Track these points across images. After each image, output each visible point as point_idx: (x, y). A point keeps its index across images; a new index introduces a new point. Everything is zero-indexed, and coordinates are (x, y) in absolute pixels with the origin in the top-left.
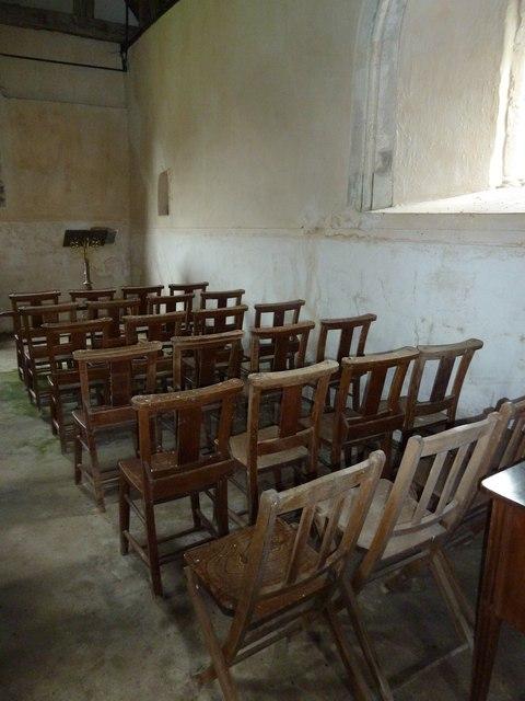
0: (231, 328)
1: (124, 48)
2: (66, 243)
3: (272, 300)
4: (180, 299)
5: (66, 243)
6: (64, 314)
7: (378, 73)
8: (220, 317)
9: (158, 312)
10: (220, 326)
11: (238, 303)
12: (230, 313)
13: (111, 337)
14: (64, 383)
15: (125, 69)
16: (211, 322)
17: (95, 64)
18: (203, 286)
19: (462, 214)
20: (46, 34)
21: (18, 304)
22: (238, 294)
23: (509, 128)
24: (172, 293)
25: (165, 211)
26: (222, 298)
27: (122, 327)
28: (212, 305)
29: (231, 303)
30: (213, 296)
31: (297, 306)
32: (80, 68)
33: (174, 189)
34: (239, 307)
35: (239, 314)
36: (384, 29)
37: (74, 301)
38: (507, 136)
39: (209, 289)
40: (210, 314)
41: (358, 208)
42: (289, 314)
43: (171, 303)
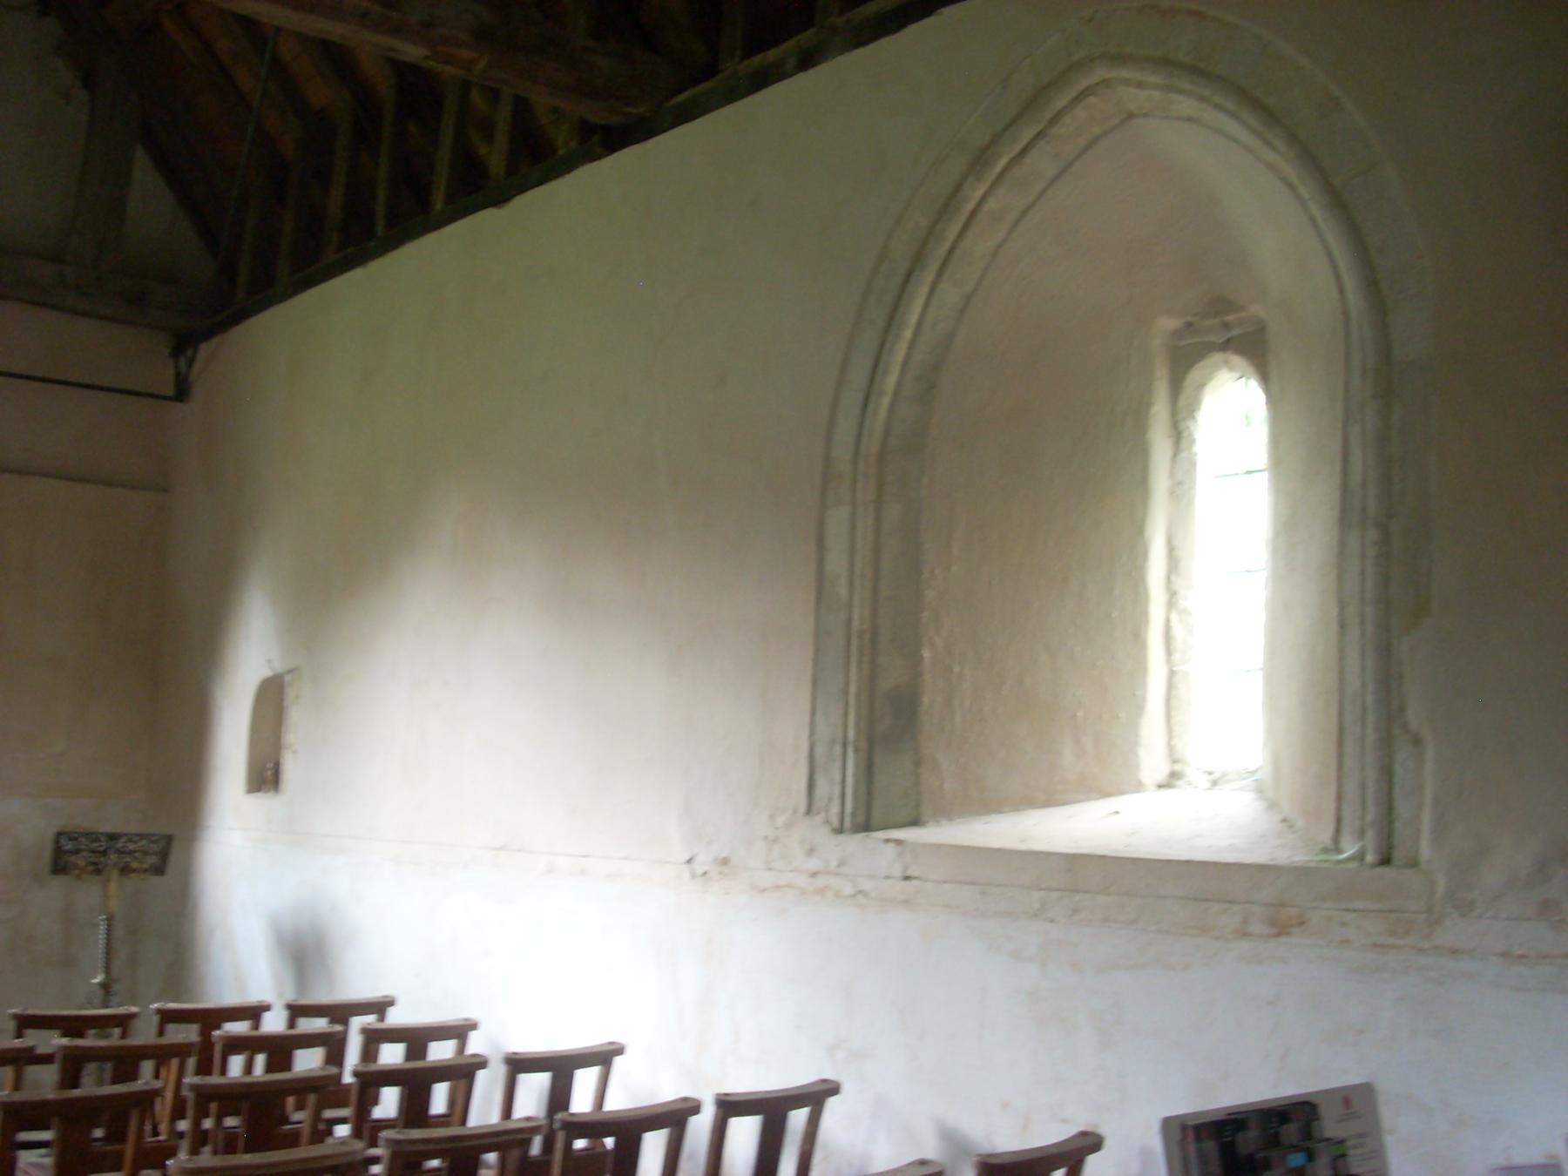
0: (443, 1120)
1: (184, 344)
2: (60, 864)
3: (744, 1083)
5: (60, 864)
7: (878, 519)
9: (223, 1071)
15: (182, 392)
18: (380, 1007)
19: (1103, 857)
20: (995, 817)
22: (460, 1032)
23: (1176, 657)
24: (292, 1024)
25: (265, 776)
26: (417, 1039)
28: (392, 1055)
30: (394, 1035)
31: (604, 1058)
32: (101, 394)
35: (463, 1073)
36: (887, 432)
38: (1172, 674)
41: (835, 822)
42: (584, 1082)
43: (280, 1050)
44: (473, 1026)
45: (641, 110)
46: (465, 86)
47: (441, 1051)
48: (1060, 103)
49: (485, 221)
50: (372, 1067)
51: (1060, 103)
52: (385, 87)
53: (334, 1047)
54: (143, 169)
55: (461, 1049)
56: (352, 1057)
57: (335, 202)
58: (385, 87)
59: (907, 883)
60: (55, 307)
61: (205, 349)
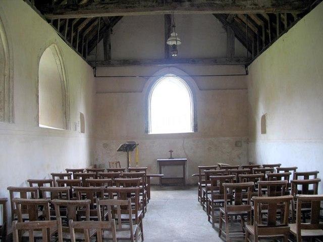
1: (246, 66)
4: (283, 175)
6: (47, 184)
8: (305, 185)
10: (305, 190)
11: (316, 177)
12: (311, 182)
13: (214, 186)
14: (216, 199)
15: (247, 74)
16: (300, 187)
17: (117, 76)
21: (201, 170)
22: (315, 174)
26: (306, 175)
27: (73, 190)
28: (301, 178)
29: (311, 178)
30: (301, 174)
33: (268, 122)
34: (316, 180)
37: (264, 168)
39: (298, 171)
40: (300, 183)
44: (297, 168)
45: (306, 9)
46: (280, 14)
47: (311, 178)
48: (113, 172)
49: (285, 35)
50: (295, 181)
51: (113, 172)
52: (267, 18)
53: (287, 177)
54: (236, 40)
55: (316, 177)
56: (291, 178)
57: (263, 38)
58: (267, 18)
59: (125, 142)
60: (226, 64)
61: (249, 67)
